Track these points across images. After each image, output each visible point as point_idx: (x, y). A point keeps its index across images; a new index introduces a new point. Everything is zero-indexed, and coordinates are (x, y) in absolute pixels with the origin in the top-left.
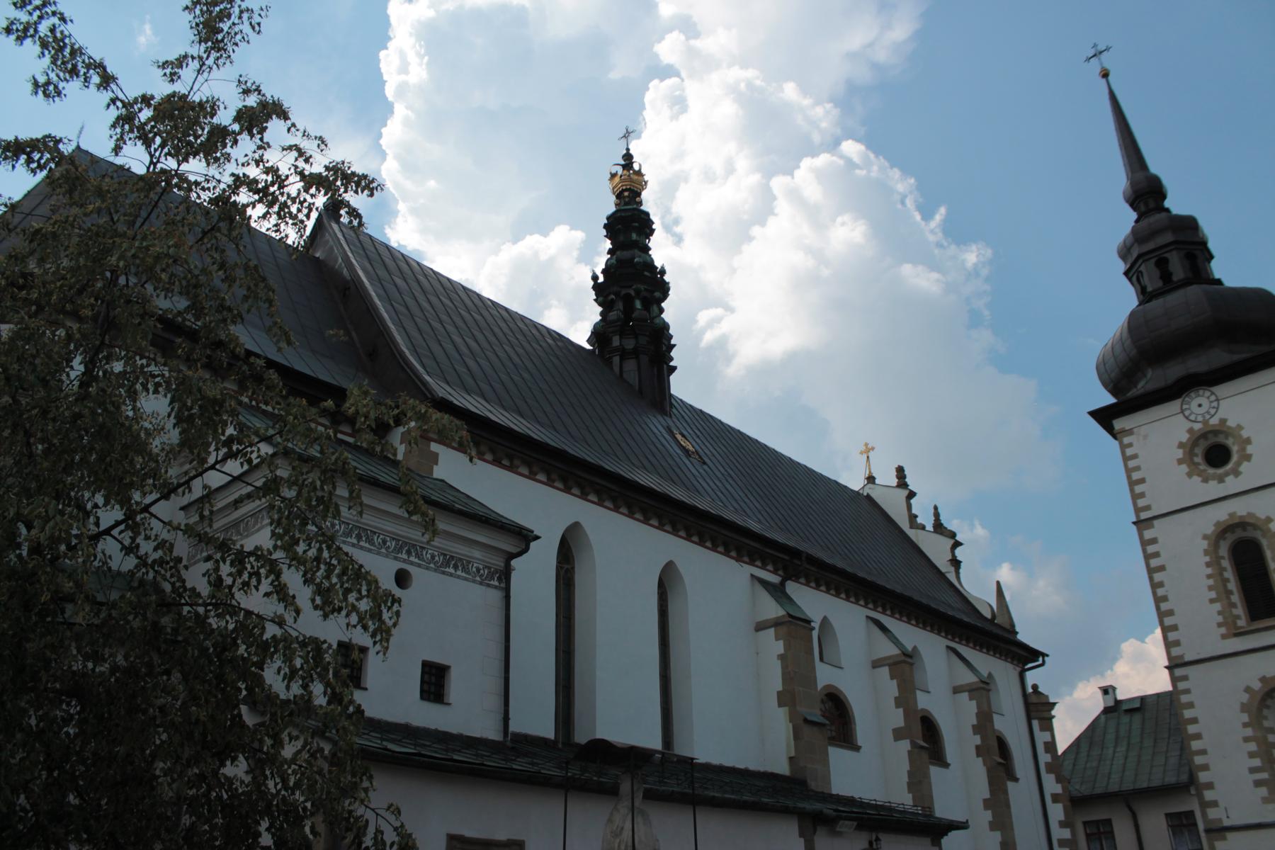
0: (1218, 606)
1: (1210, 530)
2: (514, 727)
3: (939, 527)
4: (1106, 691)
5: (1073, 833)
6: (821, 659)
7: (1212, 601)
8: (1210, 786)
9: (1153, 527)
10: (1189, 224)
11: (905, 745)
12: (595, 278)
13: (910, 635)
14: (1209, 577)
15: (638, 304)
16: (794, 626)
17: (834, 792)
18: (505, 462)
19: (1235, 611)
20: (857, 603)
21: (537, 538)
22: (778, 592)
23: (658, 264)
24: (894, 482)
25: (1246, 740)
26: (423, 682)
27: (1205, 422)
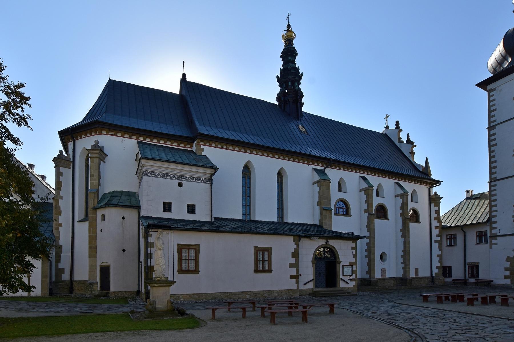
3: (409, 141)
4: (468, 192)
5: (441, 239)
9: (495, 128)
13: (375, 180)
15: (290, 84)
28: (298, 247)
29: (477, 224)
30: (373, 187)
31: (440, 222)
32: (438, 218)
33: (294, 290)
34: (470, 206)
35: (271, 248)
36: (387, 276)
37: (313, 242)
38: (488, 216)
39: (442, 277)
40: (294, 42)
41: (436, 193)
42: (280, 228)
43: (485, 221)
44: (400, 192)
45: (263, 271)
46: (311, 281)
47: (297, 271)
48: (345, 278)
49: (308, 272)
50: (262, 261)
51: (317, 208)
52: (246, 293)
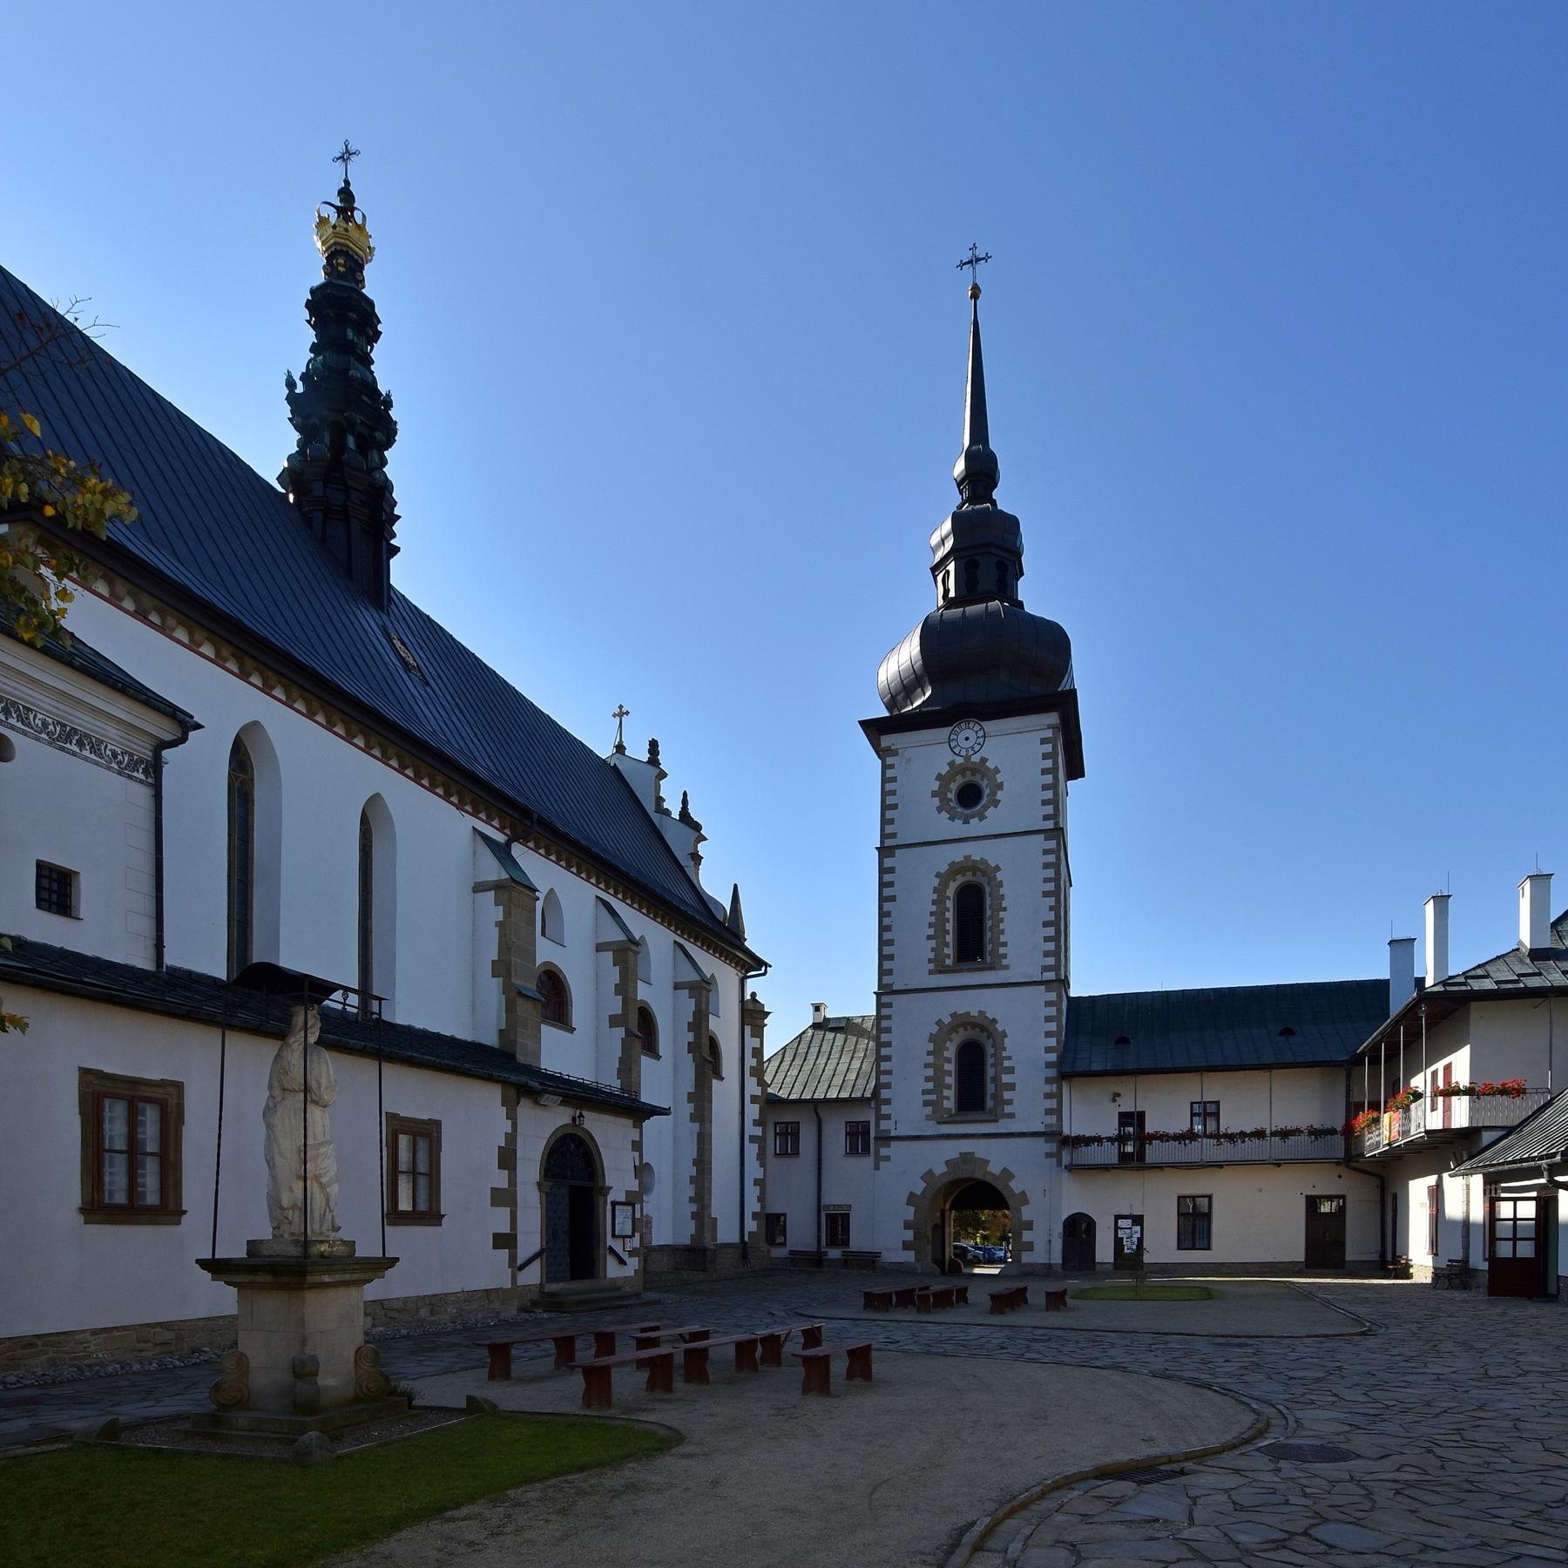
0: (933, 943)
1: (944, 869)
2: (170, 960)
3: (685, 815)
6: (543, 934)
7: (929, 937)
8: (888, 1102)
10: (1012, 524)
11: (620, 1032)
12: (290, 384)
13: (639, 923)
14: (932, 914)
16: (514, 890)
18: (154, 618)
19: (946, 951)
21: (198, 726)
22: (502, 853)
23: (382, 388)
24: (645, 757)
25: (926, 1066)
26: (39, 887)
27: (967, 758)
28: (514, 1126)
31: (762, 1083)
34: (826, 1048)
36: (655, 1243)
37: (541, 1114)
38: (872, 1084)
39: (764, 1246)
40: (368, 272)
41: (754, 995)
43: (868, 1094)
45: (132, 1212)
48: (617, 1245)
51: (496, 984)
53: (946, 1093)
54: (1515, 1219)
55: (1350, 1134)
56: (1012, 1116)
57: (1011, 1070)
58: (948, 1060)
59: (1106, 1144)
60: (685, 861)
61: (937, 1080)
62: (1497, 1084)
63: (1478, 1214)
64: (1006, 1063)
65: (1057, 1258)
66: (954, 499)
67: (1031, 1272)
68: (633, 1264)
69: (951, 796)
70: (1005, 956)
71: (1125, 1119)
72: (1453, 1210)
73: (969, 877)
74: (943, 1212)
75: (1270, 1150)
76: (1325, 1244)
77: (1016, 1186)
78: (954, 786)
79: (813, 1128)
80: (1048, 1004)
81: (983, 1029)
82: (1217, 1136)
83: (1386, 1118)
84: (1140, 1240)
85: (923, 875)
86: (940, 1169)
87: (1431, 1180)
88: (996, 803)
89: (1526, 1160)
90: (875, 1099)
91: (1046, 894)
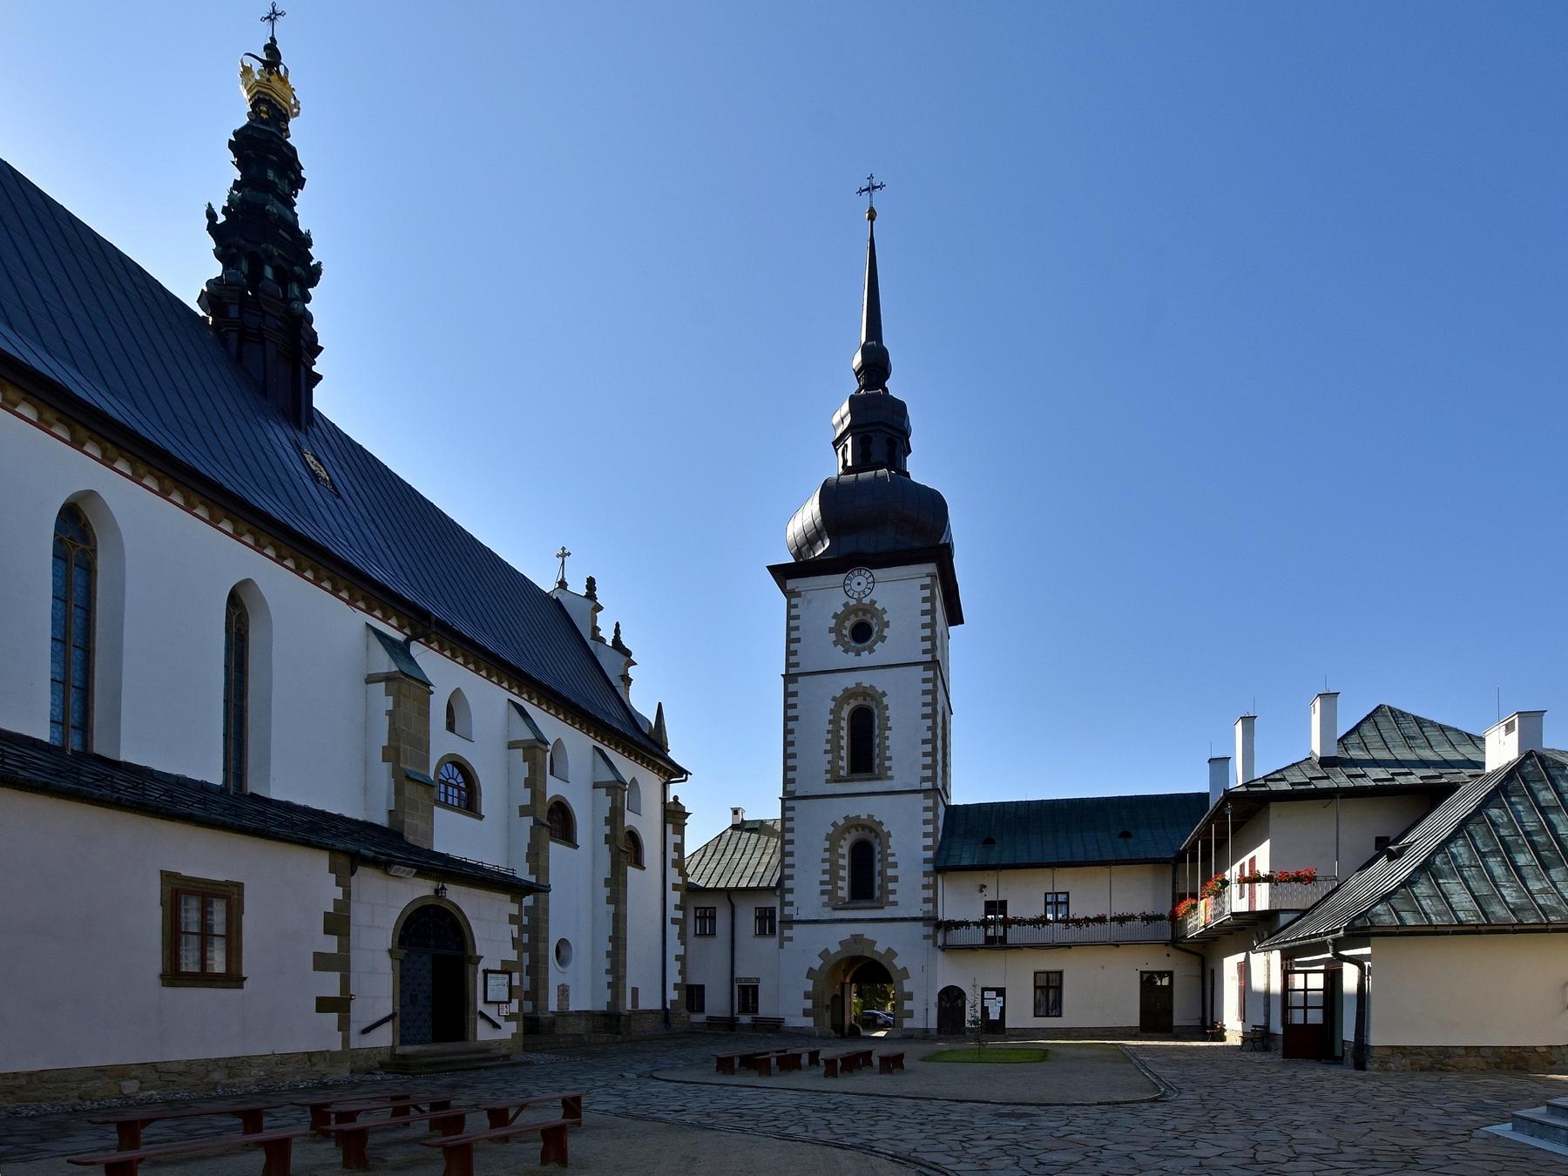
0: (829, 757)
1: (839, 694)
3: (617, 642)
6: (451, 727)
7: (826, 752)
8: (791, 891)
10: (900, 408)
12: (211, 215)
13: (551, 726)
17: (438, 847)
20: (499, 684)
22: (398, 650)
23: (303, 228)
24: (584, 592)
25: (824, 861)
27: (859, 600)
29: (757, 889)
30: (547, 743)
31: (683, 873)
32: (680, 864)
33: (333, 1054)
35: (240, 886)
37: (393, 884)
39: (684, 1012)
40: (293, 124)
41: (676, 798)
42: (235, 808)
43: (773, 884)
44: (610, 777)
45: (203, 978)
46: (386, 1020)
47: (345, 983)
48: (491, 1012)
49: (377, 987)
50: (199, 935)
51: (385, 769)
52: (119, 1073)
53: (840, 884)
54: (1306, 990)
55: (1176, 922)
56: (895, 903)
57: (895, 865)
58: (843, 856)
59: (973, 927)
60: (616, 682)
61: (833, 872)
62: (1292, 873)
63: (1276, 987)
64: (891, 859)
65: (933, 1024)
66: (853, 386)
67: (910, 1036)
68: (509, 1030)
69: (846, 632)
70: (890, 768)
71: (990, 907)
72: (1258, 983)
73: (860, 701)
74: (843, 985)
75: (1111, 932)
76: (1156, 1012)
77: (899, 963)
78: (848, 624)
79: (727, 912)
80: (926, 809)
81: (871, 830)
82: (1067, 921)
83: (1202, 904)
84: (1003, 1009)
85: (822, 696)
86: (835, 948)
87: (1241, 957)
88: (883, 639)
89: (1314, 936)
90: (780, 888)
91: (925, 716)
